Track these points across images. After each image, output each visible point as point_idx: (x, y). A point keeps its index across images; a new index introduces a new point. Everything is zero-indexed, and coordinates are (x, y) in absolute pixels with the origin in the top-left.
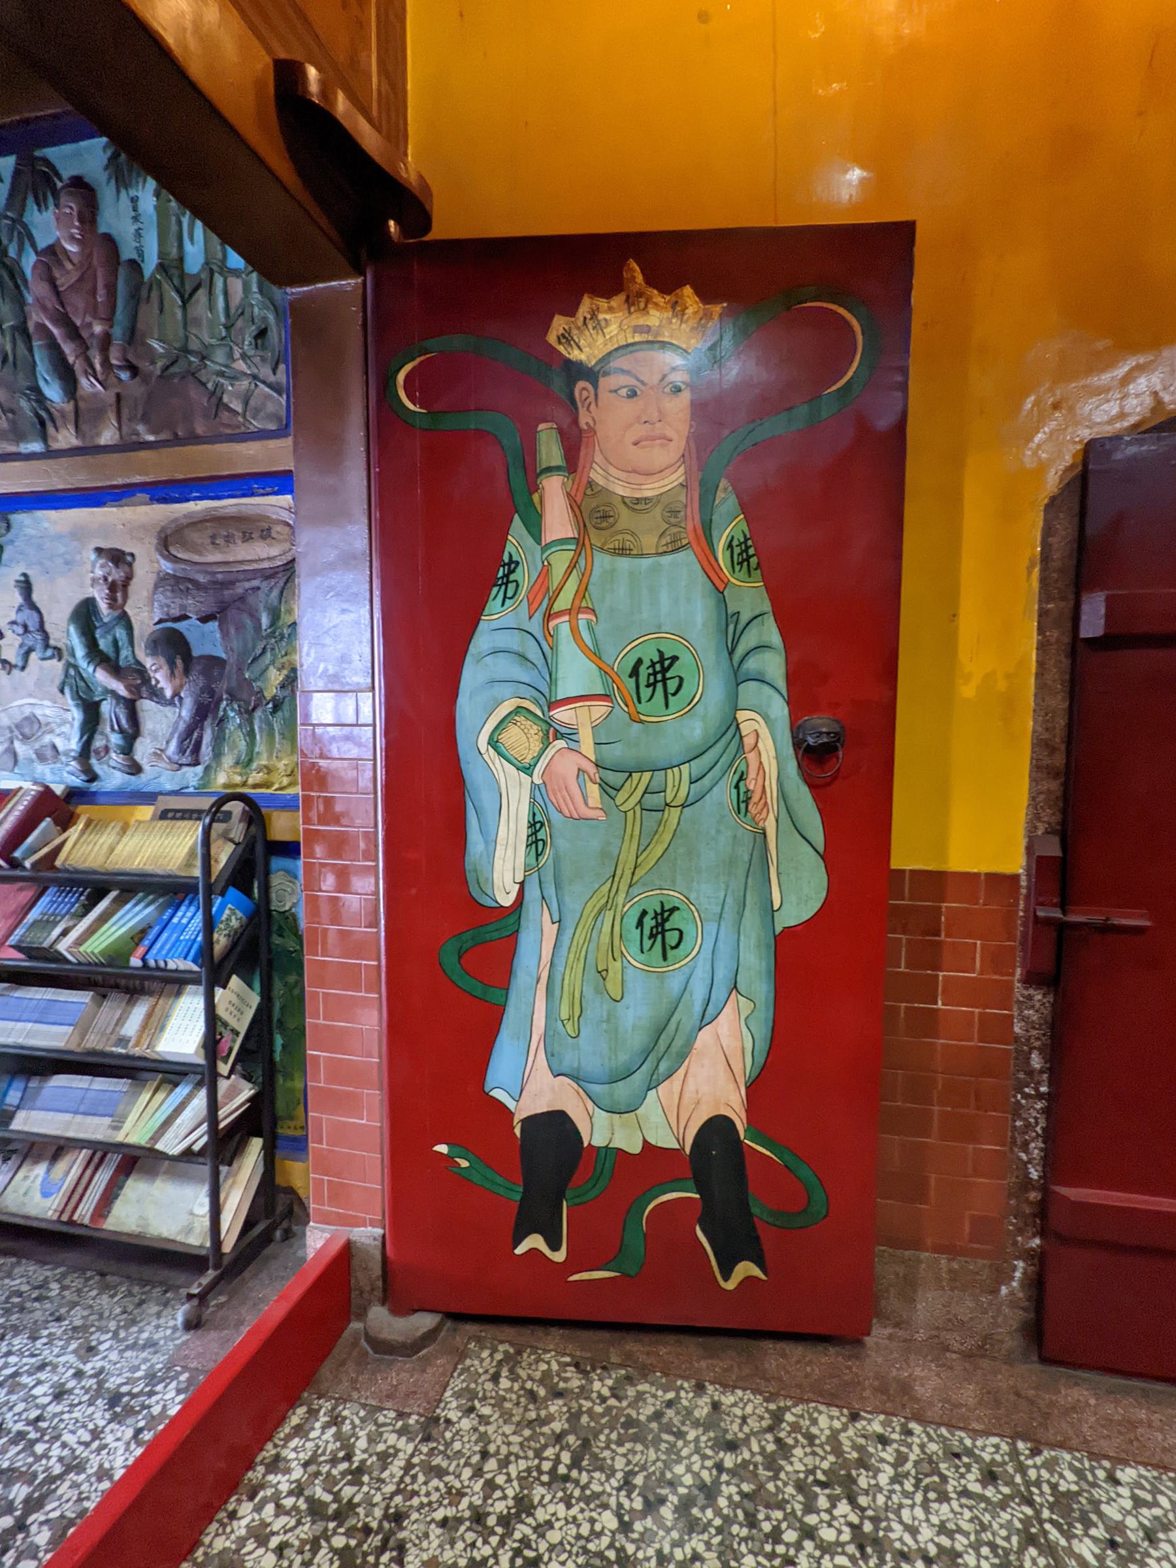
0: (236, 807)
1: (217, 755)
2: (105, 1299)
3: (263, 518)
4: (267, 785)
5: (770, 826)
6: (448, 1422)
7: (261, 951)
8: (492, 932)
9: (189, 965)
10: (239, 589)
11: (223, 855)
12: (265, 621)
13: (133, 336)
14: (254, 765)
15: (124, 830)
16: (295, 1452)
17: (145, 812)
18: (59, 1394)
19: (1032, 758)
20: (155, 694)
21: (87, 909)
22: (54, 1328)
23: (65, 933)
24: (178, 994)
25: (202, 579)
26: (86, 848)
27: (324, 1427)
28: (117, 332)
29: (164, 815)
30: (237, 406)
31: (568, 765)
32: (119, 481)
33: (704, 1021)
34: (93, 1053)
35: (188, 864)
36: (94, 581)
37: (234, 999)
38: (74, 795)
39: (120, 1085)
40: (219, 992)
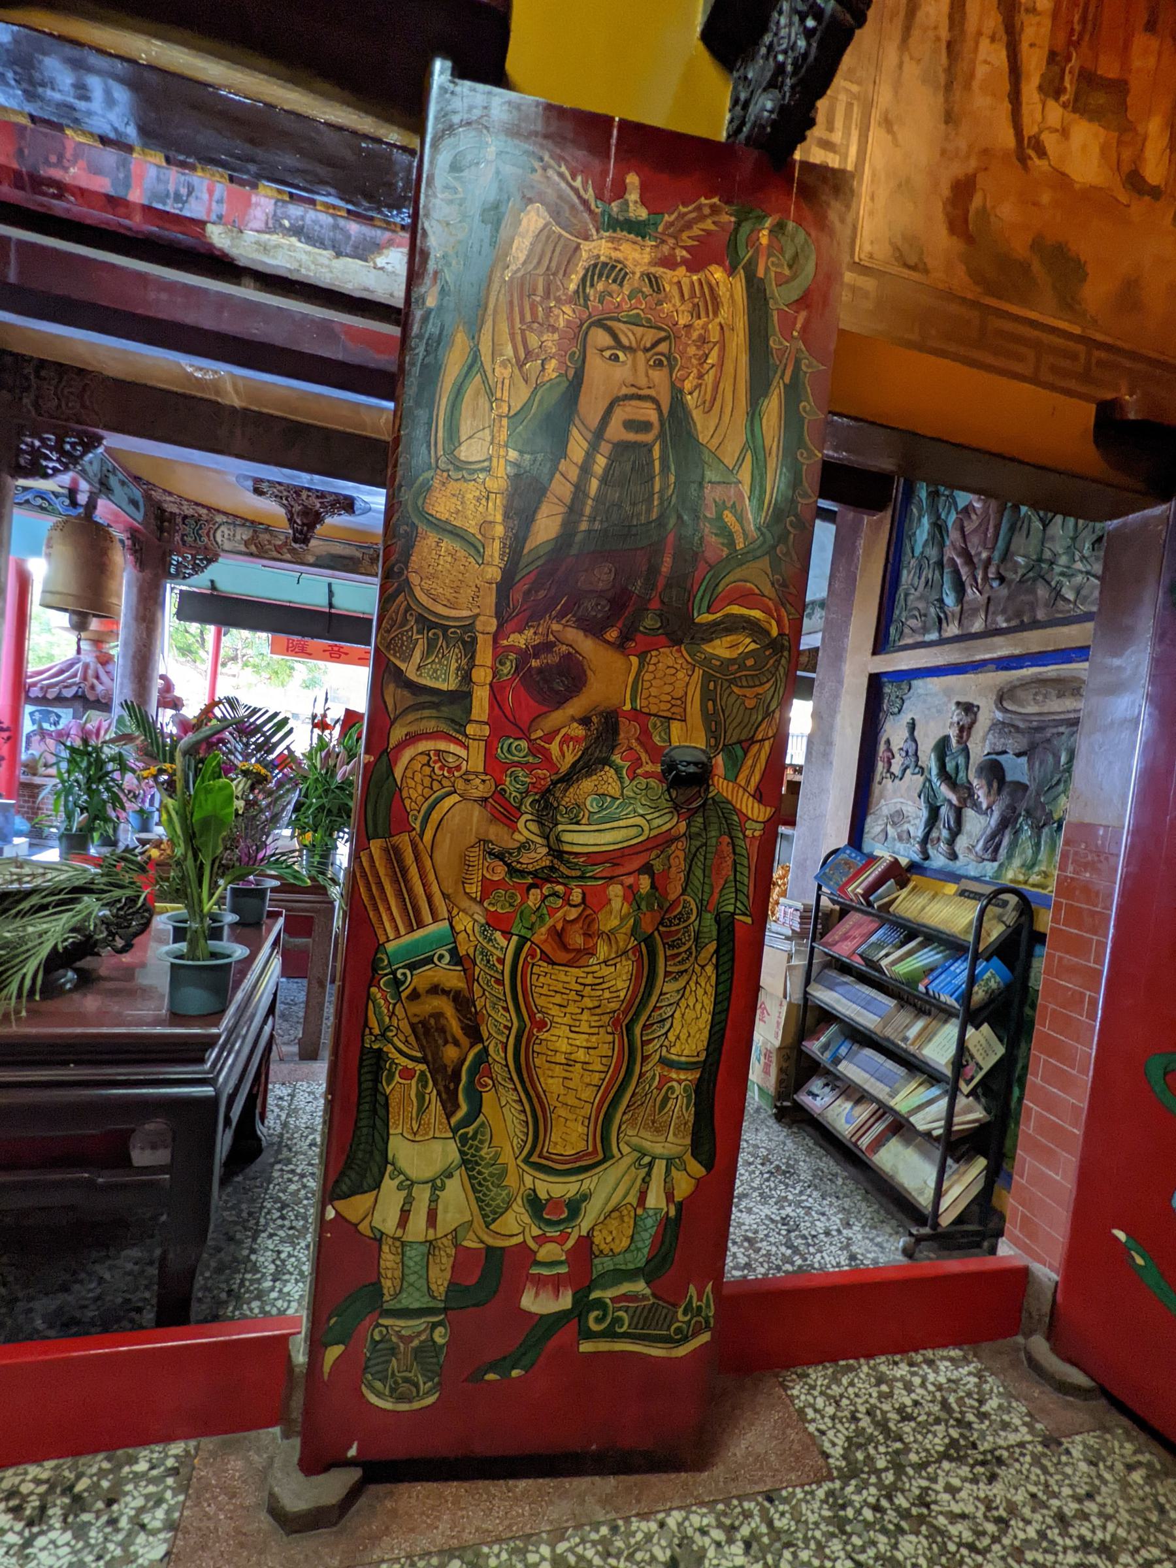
0: (1013, 899)
1: (1010, 856)
2: (864, 1205)
3: (1076, 679)
4: (1043, 886)
6: (1068, 1452)
7: (1010, 1013)
9: (951, 1001)
10: (1048, 733)
11: (994, 932)
12: (1063, 759)
13: (1006, 555)
14: (1036, 869)
15: (934, 897)
16: (944, 1372)
17: (951, 888)
18: (827, 1233)
20: (976, 806)
21: (903, 944)
22: (834, 1200)
23: (887, 955)
24: (946, 1022)
25: (1022, 725)
26: (911, 904)
27: (970, 1374)
28: (997, 555)
29: (963, 893)
30: (1071, 596)
32: (978, 658)
34: (888, 1039)
35: (967, 932)
36: (952, 724)
37: (983, 1042)
38: (913, 867)
39: (901, 1071)
40: (970, 1031)
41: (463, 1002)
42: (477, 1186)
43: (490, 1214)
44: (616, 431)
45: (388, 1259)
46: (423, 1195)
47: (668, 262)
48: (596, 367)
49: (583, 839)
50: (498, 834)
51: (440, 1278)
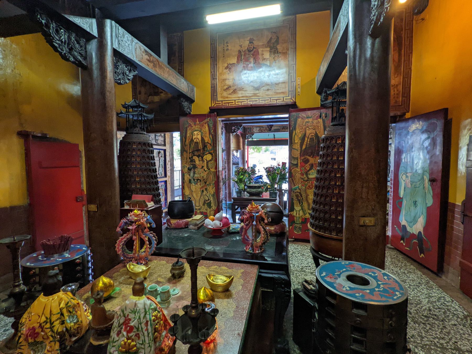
5: (427, 191)
8: (401, 200)
19: (142, 194)
31: (408, 181)
33: (419, 217)
41: (300, 193)
42: (303, 212)
43: (305, 215)
44: (310, 137)
45: (295, 218)
46: (298, 212)
47: (314, 120)
48: (307, 131)
49: (311, 176)
50: (302, 177)
51: (300, 221)
